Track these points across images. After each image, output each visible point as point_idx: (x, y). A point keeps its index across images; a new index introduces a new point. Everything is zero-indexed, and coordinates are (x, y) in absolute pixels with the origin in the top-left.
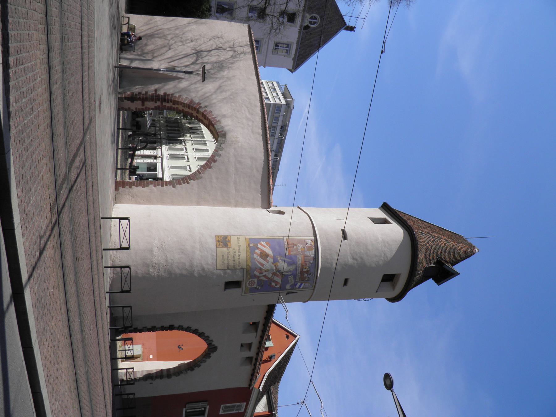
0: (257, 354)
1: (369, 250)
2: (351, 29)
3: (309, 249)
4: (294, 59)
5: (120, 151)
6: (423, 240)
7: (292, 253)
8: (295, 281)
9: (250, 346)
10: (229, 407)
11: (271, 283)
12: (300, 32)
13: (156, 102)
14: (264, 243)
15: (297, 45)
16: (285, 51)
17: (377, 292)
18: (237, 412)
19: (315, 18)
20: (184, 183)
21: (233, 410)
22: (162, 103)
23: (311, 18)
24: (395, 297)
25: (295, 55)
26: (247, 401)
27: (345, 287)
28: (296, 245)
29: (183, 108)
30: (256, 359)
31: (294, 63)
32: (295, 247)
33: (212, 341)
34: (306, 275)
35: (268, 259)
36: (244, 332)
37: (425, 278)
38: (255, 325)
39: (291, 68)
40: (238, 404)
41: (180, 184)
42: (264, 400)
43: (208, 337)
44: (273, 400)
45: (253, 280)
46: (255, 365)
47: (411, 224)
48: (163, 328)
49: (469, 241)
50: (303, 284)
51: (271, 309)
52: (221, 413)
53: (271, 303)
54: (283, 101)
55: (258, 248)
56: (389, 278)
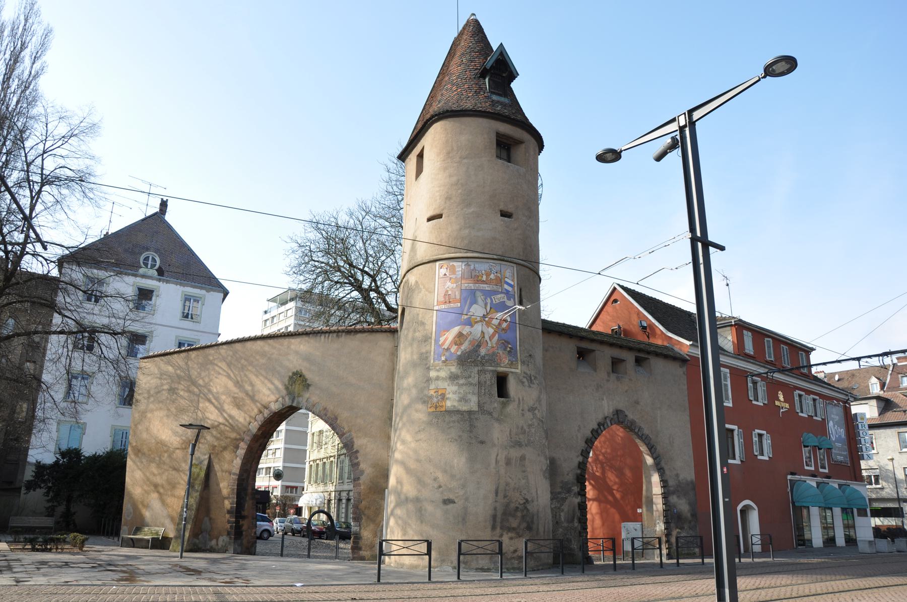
0: (630, 349)
1: (458, 181)
2: (164, 205)
3: (453, 270)
6: (449, 98)
7: (458, 297)
8: (502, 293)
11: (503, 329)
12: (167, 282)
18: (729, 380)
19: (147, 259)
23: (146, 265)
25: (201, 288)
28: (447, 291)
30: (640, 350)
31: (214, 291)
32: (450, 293)
34: (492, 276)
35: (465, 333)
37: (510, 94)
38: (582, 354)
46: (649, 353)
47: (428, 116)
49: (460, 28)
52: (730, 405)
53: (540, 326)
56: (505, 147)
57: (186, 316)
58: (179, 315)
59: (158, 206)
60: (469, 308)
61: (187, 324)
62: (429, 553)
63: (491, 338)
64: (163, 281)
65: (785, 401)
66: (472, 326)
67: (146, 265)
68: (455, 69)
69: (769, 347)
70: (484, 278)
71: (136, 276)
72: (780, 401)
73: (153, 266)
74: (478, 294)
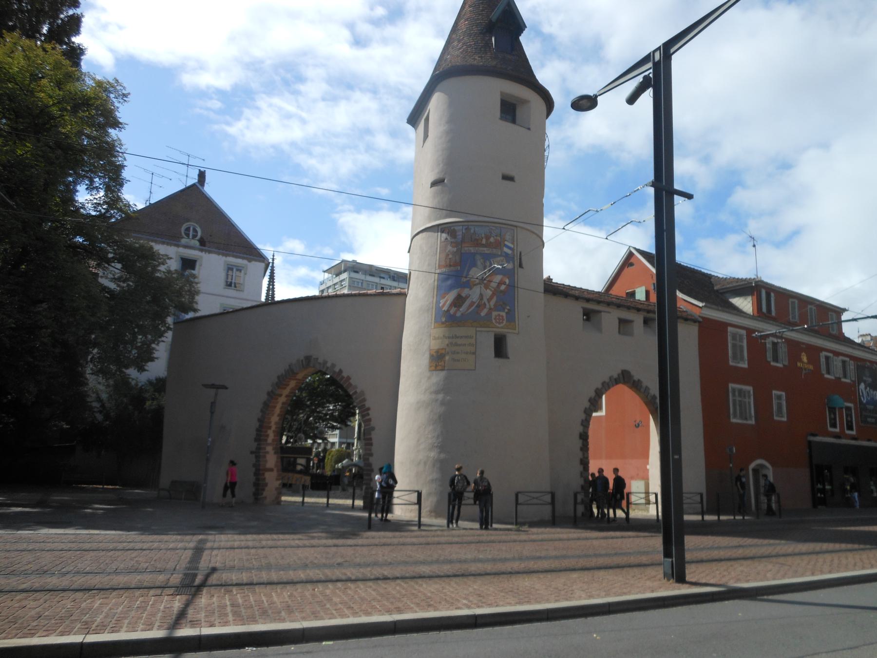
0: (639, 310)
2: (202, 176)
4: (250, 261)
5: (331, 501)
8: (501, 256)
9: (622, 322)
10: (734, 354)
11: (501, 291)
12: (210, 252)
13: (268, 452)
14: (442, 302)
15: (229, 255)
16: (238, 273)
17: (529, 129)
19: (188, 229)
20: (368, 414)
21: (741, 347)
22: (269, 444)
24: (543, 99)
25: (243, 258)
26: (723, 326)
27: (516, 179)
29: (276, 415)
31: (256, 260)
33: (610, 378)
34: (492, 240)
35: (463, 295)
36: (599, 329)
38: (588, 315)
39: (263, 265)
40: (729, 338)
41: (370, 420)
42: (738, 301)
43: (603, 383)
44: (735, 284)
45: (493, 317)
48: (585, 448)
50: (506, 243)
51: (553, 289)
54: (345, 276)
55: (448, 311)
56: (509, 110)
57: (229, 285)
58: (222, 283)
59: (197, 177)
60: (469, 271)
61: (231, 292)
62: (419, 502)
63: (489, 300)
64: (206, 251)
65: (809, 362)
66: (471, 289)
67: (188, 235)
68: (463, 25)
69: (794, 308)
70: (484, 241)
71: (178, 246)
72: (803, 362)
73: (194, 237)
74: (478, 257)
